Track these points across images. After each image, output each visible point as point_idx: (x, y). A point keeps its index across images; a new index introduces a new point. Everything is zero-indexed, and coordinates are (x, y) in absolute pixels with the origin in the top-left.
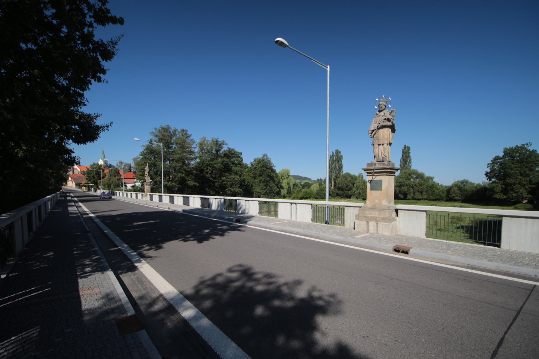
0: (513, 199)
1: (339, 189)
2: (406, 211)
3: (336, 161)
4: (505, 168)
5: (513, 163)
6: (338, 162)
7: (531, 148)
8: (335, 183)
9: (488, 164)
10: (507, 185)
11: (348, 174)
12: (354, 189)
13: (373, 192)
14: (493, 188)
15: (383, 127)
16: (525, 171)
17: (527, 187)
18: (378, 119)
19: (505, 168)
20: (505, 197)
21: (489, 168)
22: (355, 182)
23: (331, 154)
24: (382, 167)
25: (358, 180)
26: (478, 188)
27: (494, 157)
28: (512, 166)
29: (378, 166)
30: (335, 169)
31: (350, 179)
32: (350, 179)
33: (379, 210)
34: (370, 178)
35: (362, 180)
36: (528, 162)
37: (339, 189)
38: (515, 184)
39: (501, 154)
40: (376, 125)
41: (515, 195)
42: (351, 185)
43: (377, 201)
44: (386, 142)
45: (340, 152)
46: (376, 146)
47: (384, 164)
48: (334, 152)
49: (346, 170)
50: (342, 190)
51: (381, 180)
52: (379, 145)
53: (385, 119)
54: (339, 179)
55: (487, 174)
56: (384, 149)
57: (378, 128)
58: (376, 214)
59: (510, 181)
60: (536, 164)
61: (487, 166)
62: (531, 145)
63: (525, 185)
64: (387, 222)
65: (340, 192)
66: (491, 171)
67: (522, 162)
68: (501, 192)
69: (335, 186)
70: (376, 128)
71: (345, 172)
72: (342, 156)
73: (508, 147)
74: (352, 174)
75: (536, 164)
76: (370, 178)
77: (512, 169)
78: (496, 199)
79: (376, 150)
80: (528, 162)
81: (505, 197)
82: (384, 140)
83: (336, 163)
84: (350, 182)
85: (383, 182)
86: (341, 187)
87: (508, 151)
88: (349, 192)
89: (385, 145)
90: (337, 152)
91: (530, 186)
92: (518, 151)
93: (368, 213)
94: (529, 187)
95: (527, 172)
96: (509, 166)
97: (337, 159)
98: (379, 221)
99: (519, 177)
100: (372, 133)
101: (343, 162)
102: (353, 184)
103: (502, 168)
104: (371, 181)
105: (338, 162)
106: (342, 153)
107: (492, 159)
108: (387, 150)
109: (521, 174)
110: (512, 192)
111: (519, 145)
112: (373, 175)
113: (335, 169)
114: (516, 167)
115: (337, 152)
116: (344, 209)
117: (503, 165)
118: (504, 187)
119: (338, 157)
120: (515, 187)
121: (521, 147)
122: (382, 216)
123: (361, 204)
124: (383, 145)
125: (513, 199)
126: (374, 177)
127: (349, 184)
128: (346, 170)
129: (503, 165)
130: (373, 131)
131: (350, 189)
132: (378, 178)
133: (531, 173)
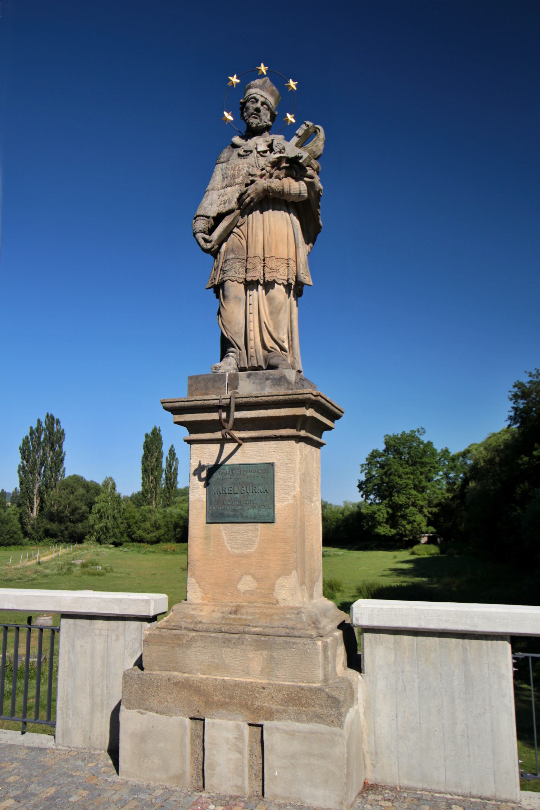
0: (406, 536)
1: (52, 517)
2: (406, 639)
3: (44, 446)
4: (391, 474)
5: (401, 465)
6: (52, 448)
7: (425, 439)
8: (42, 501)
9: (362, 466)
10: (396, 507)
11: (77, 479)
12: (92, 518)
13: (223, 530)
14: (374, 513)
15: (270, 200)
16: (420, 481)
17: (425, 510)
18: (244, 166)
19: (391, 474)
20: (394, 531)
21: (364, 473)
22: (96, 499)
23: (35, 426)
24: (269, 391)
25: (102, 496)
26: (347, 513)
27: (370, 451)
28: (401, 470)
29: (247, 388)
30: (42, 464)
31: (81, 491)
32: (81, 491)
33: (265, 640)
34: (208, 454)
35: (112, 493)
36: (422, 463)
37: (52, 517)
38: (407, 506)
39: (382, 447)
40: (233, 193)
41: (409, 527)
42: (84, 508)
43: (247, 584)
44: (282, 274)
45: (58, 422)
46: (235, 289)
47: (282, 380)
48: (43, 420)
49: (71, 468)
50: (61, 521)
51: (268, 469)
52: (250, 285)
53: (276, 164)
54: (54, 493)
55: (360, 486)
56: (274, 312)
57: (245, 207)
58: (247, 668)
59: (400, 499)
60: (434, 468)
61: (359, 469)
62: (424, 432)
63: (422, 507)
64: (318, 718)
65: (54, 526)
66: (368, 480)
67: (414, 464)
68: (387, 523)
69: (41, 509)
70: (233, 204)
71: (68, 474)
72: (63, 433)
73: (391, 434)
74: (88, 478)
75: (434, 468)
76: (208, 454)
77: (400, 477)
78: (378, 535)
79: (234, 311)
80: (423, 464)
81: (394, 531)
82: (271, 264)
83: (47, 449)
84: (81, 498)
85: (279, 475)
86: (59, 512)
87: (392, 443)
88: (80, 525)
89: (279, 291)
90: (51, 420)
91: (430, 510)
92: (407, 441)
93: (200, 664)
94: (430, 513)
95: (424, 483)
96: (396, 471)
97: (49, 439)
98: (270, 715)
99: (414, 492)
100: (210, 231)
101: (65, 448)
102: (90, 505)
103: (385, 474)
104: (213, 470)
105: (52, 448)
106: (64, 426)
107: (367, 456)
108: (284, 318)
109: (415, 487)
110: (404, 523)
111: (408, 432)
112: (222, 442)
113: (42, 464)
114: (407, 474)
115: (51, 420)
116: (55, 631)
117: (386, 468)
118: (390, 511)
119: (51, 433)
120: (408, 511)
121: (410, 435)
122: (284, 679)
123: (153, 602)
124: (268, 286)
125: (406, 536)
126: (229, 447)
127: (78, 504)
128: (71, 468)
129: (386, 468)
130: (219, 218)
131: (83, 518)
132: (251, 454)
133: (429, 484)
